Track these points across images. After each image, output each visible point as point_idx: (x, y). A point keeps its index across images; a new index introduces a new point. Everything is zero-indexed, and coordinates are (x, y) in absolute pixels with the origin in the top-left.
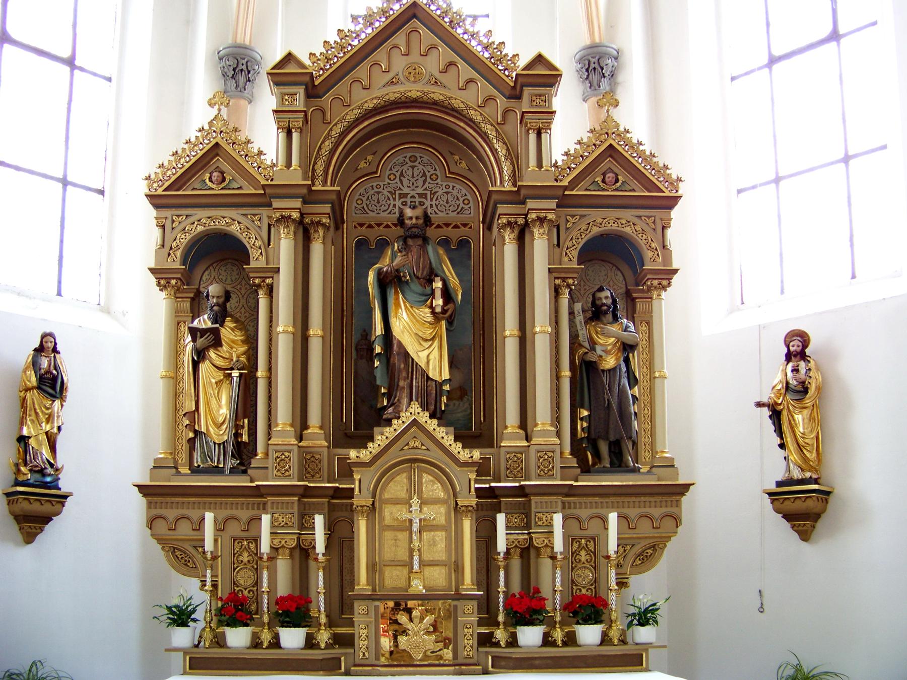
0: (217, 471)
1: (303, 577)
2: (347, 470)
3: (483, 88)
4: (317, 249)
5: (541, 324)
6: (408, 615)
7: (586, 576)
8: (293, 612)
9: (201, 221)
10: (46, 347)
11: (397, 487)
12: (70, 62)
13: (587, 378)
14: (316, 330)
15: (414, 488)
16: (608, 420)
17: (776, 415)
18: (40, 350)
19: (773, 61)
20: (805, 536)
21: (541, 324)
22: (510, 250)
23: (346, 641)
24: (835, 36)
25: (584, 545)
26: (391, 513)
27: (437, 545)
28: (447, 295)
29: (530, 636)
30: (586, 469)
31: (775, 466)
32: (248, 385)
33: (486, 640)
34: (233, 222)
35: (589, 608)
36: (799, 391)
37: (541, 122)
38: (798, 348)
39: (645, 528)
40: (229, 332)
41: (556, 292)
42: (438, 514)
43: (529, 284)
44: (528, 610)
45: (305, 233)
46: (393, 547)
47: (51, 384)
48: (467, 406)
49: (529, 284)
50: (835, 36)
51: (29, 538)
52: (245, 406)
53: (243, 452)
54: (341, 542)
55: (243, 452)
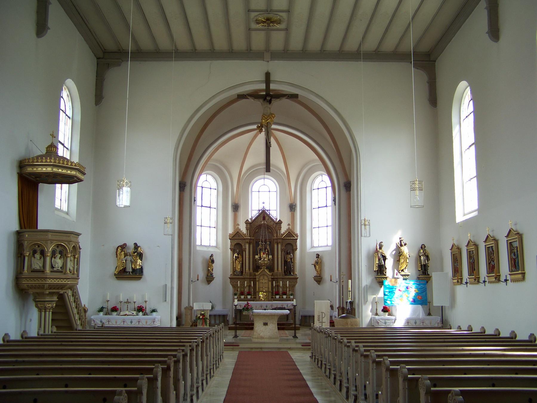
0: (238, 275)
1: (249, 289)
2: (255, 275)
3: (272, 223)
4: (251, 246)
5: (280, 256)
6: (424, 77)
7: (285, 289)
8: (249, 294)
9: (236, 242)
10: (212, 256)
11: (262, 278)
12: (210, 207)
13: (286, 263)
14: (251, 257)
15: (264, 278)
16: (289, 268)
17: (315, 266)
18: (211, 256)
19: (319, 207)
20: (319, 284)
21: (280, 256)
22: (276, 246)
23: (255, 298)
24: (326, 206)
25: (284, 285)
26: (261, 281)
27: (266, 285)
28: (268, 251)
29: (278, 297)
30: (286, 275)
31: (315, 273)
32: (242, 264)
33: (272, 298)
34: (240, 242)
35: (285, 293)
36: (317, 263)
37: (280, 228)
38: (318, 256)
39: (293, 283)
40: (239, 256)
41: (282, 252)
42: (266, 281)
43: (279, 249)
44: (277, 294)
45: (250, 244)
46: (261, 285)
47: (213, 261)
48: (271, 268)
49: (279, 249)
50: (326, 206)
51: (209, 284)
52: (242, 266)
53: (242, 272)
54: (255, 284)
55: (242, 272)
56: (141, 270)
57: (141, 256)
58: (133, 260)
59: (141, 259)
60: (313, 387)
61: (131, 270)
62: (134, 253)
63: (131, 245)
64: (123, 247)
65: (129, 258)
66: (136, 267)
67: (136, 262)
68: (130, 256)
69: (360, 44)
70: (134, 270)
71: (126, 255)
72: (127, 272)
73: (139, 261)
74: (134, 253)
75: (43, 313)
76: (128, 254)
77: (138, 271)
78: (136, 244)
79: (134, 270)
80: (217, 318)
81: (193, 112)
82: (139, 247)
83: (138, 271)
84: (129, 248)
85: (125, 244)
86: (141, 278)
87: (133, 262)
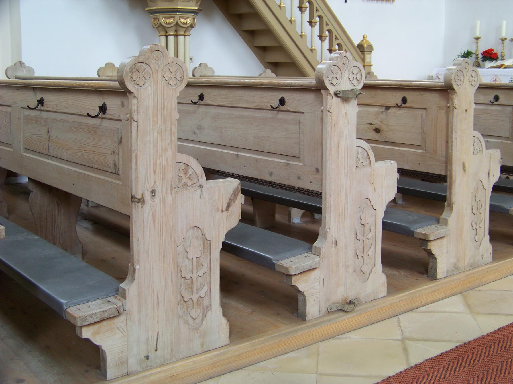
75: (171, 39)
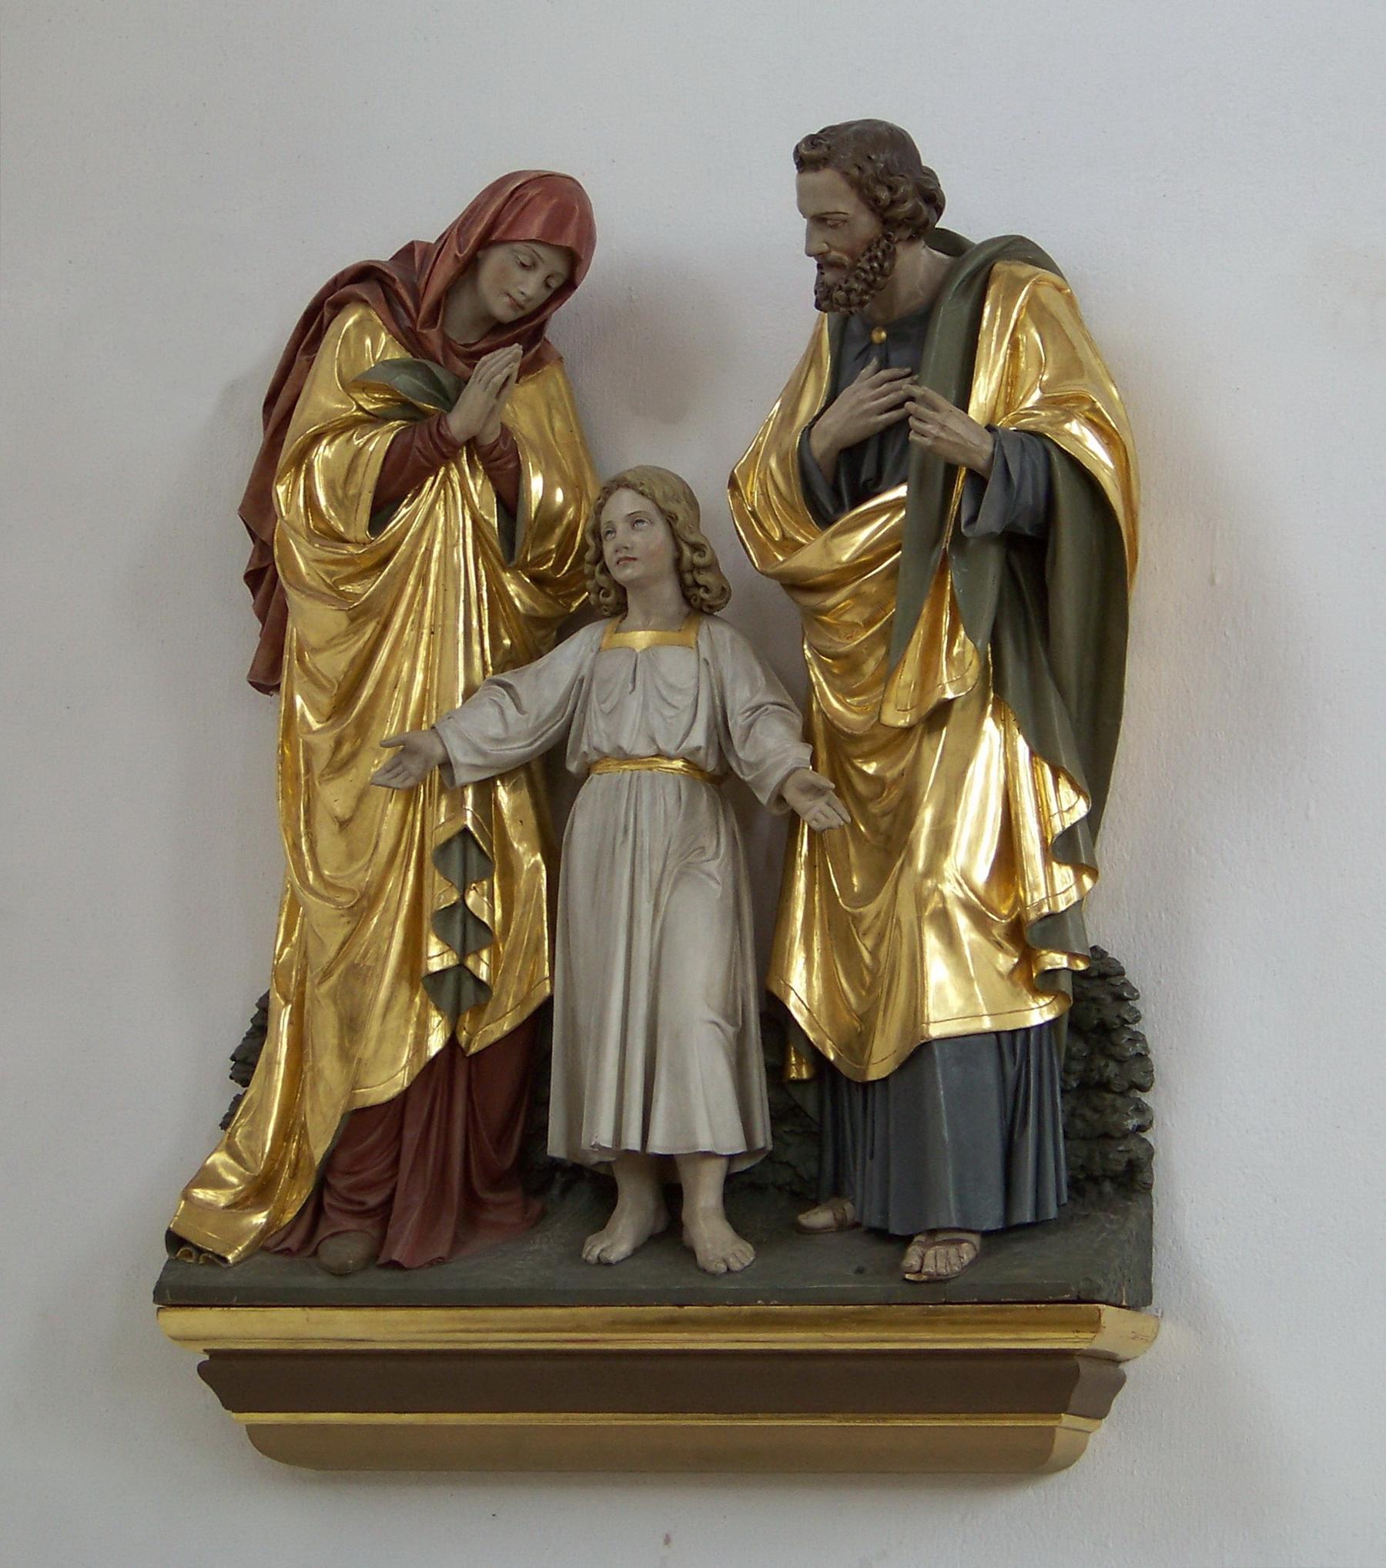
56: (1084, 1081)
57: (1048, 579)
58: (774, 751)
59: (1083, 733)
60: (520, 842)
61: (707, 1112)
62: (835, 481)
63: (713, 238)
64: (474, 309)
65: (653, 688)
66: (874, 974)
67: (887, 833)
68: (698, 597)
69: (383, 1237)
70: (826, 1124)
71: (559, 588)
72: (594, 1186)
73: (990, 786)
74: (835, 481)
76: (639, 547)
77: (961, 1128)
78: (870, 182)
79: (826, 1124)
80: (877, 1086)
81: (660, 1021)
82: (980, 271)
83: (961, 1128)
84: (669, 362)
85: (539, 219)
86: (1073, 1385)
87: (797, 833)
